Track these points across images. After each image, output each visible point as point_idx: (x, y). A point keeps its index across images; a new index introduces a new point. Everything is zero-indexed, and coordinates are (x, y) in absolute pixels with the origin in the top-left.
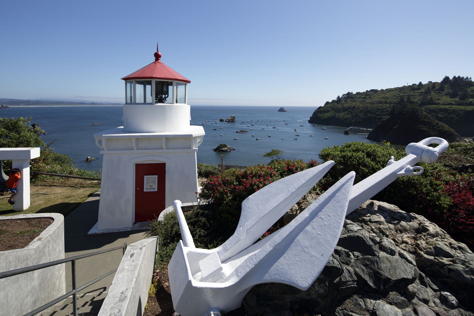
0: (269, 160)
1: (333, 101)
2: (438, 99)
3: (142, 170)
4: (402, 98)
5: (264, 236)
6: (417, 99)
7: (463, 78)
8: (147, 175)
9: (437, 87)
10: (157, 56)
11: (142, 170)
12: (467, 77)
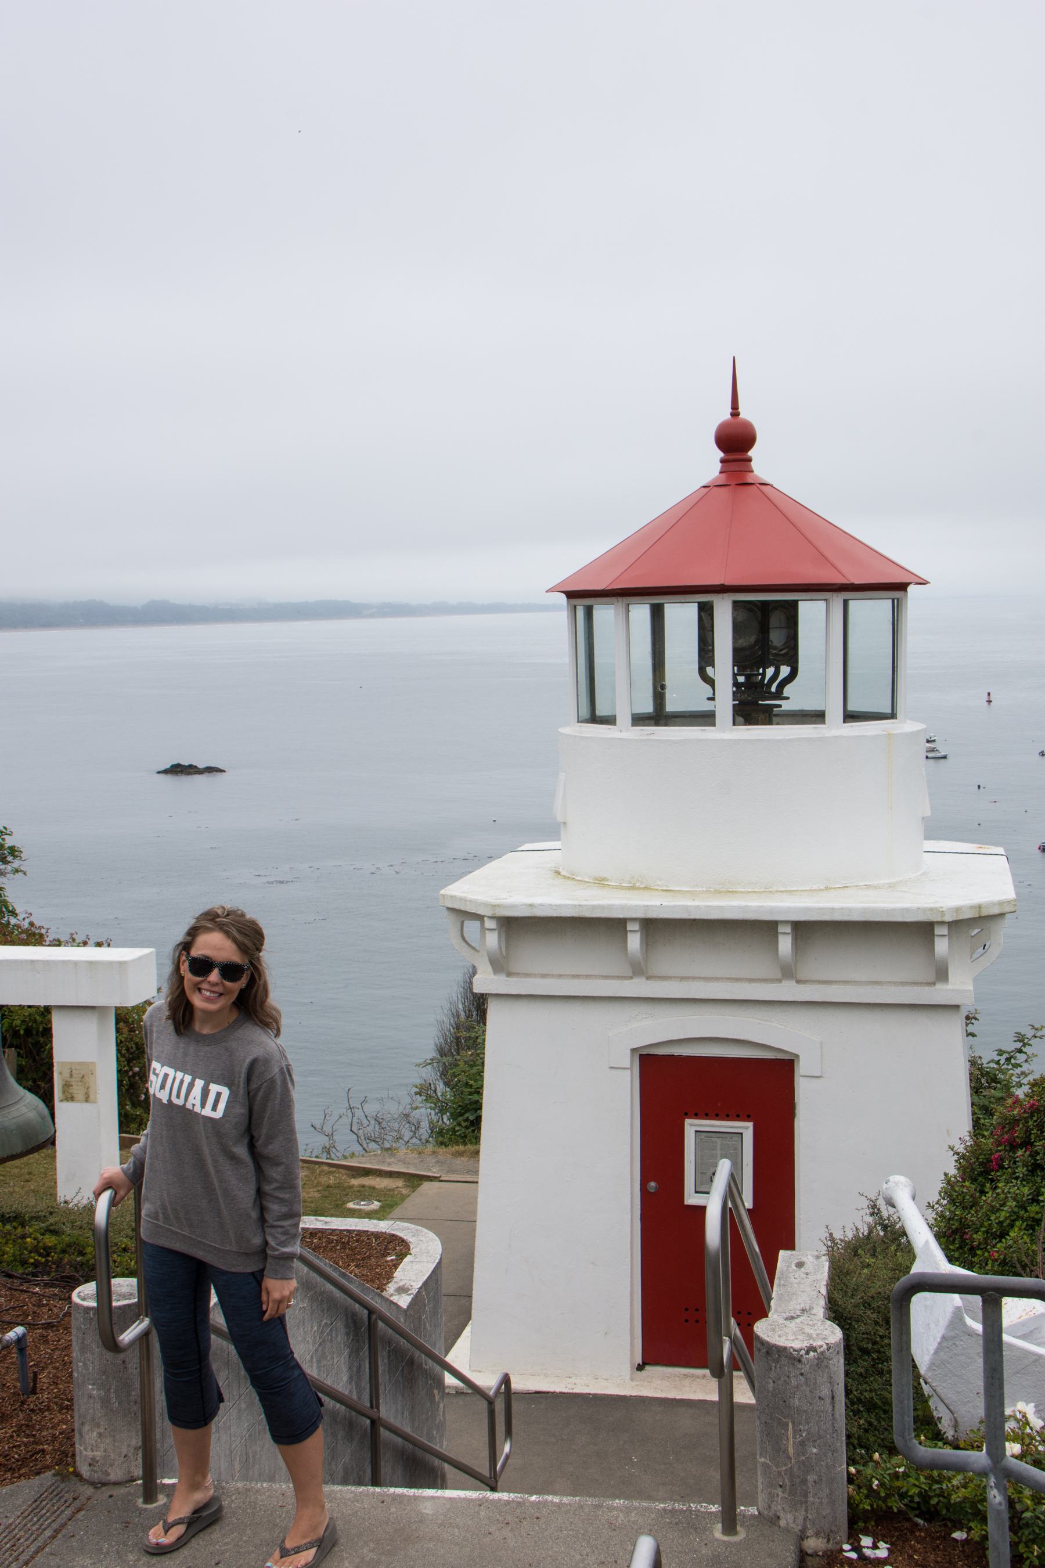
3: (676, 1090)
10: (736, 442)
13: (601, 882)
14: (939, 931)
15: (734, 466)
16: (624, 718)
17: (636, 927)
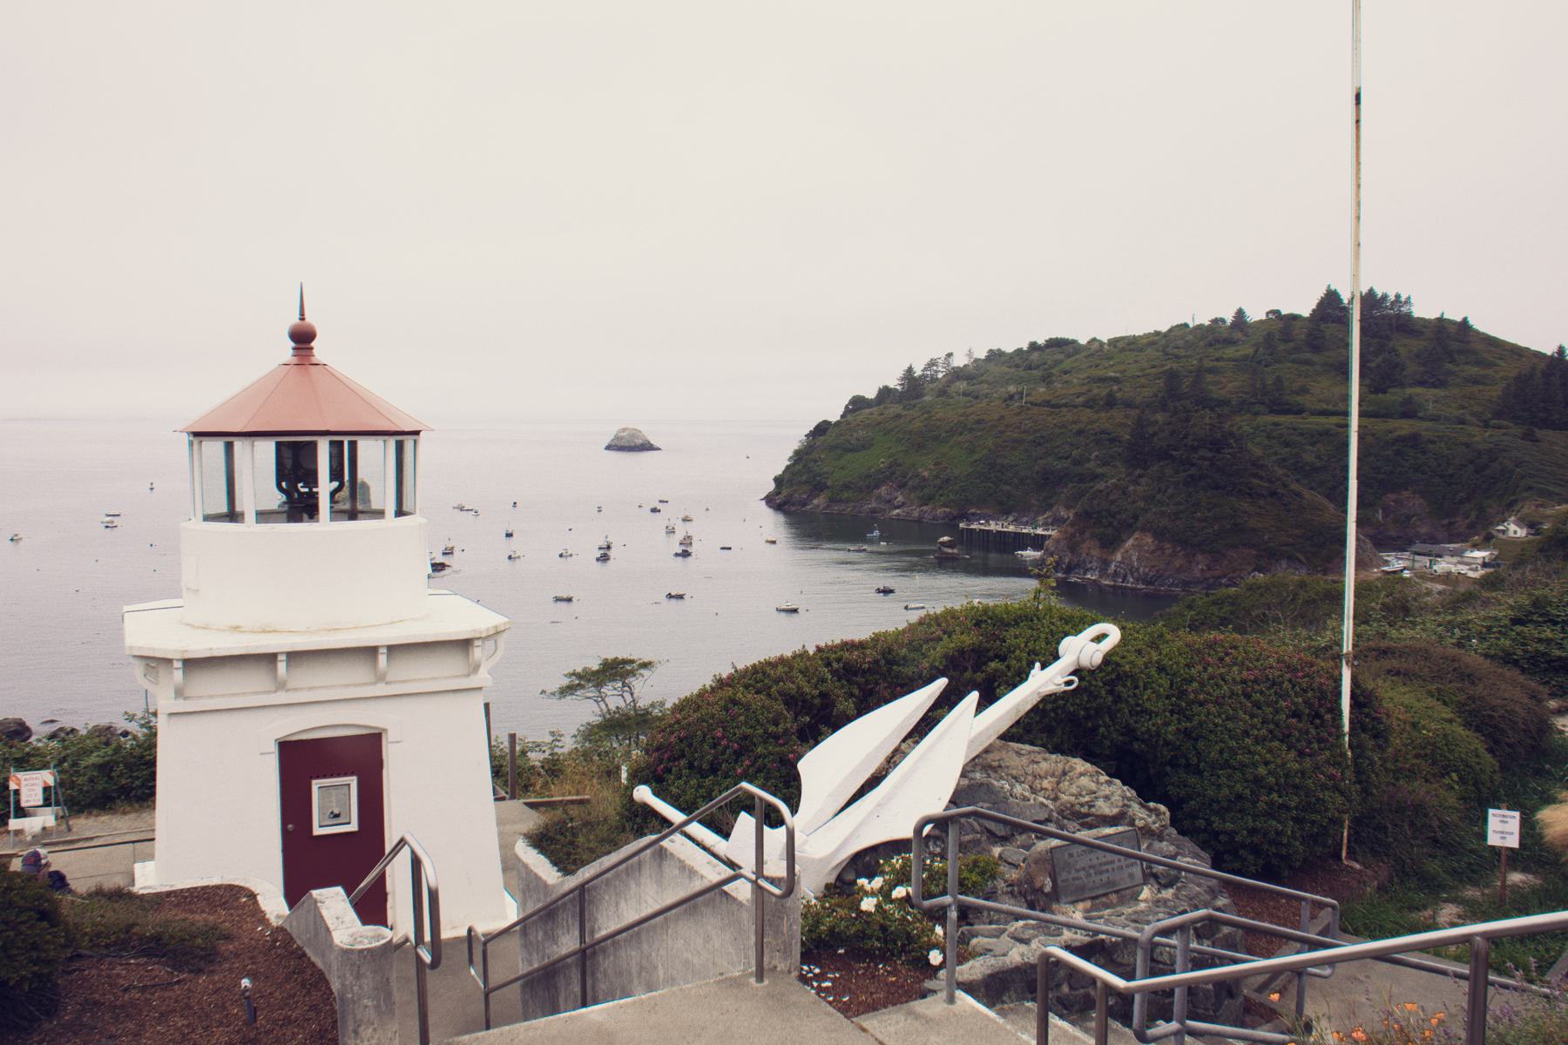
0: (585, 711)
1: (885, 392)
2: (1303, 390)
3: (302, 762)
4: (1172, 376)
5: (843, 809)
6: (1229, 386)
7: (1385, 297)
8: (318, 777)
9: (1300, 334)
10: (303, 338)
11: (302, 762)
12: (1398, 296)
13: (236, 629)
14: (280, 658)
15: (303, 352)
16: (250, 516)
17: (179, 665)
